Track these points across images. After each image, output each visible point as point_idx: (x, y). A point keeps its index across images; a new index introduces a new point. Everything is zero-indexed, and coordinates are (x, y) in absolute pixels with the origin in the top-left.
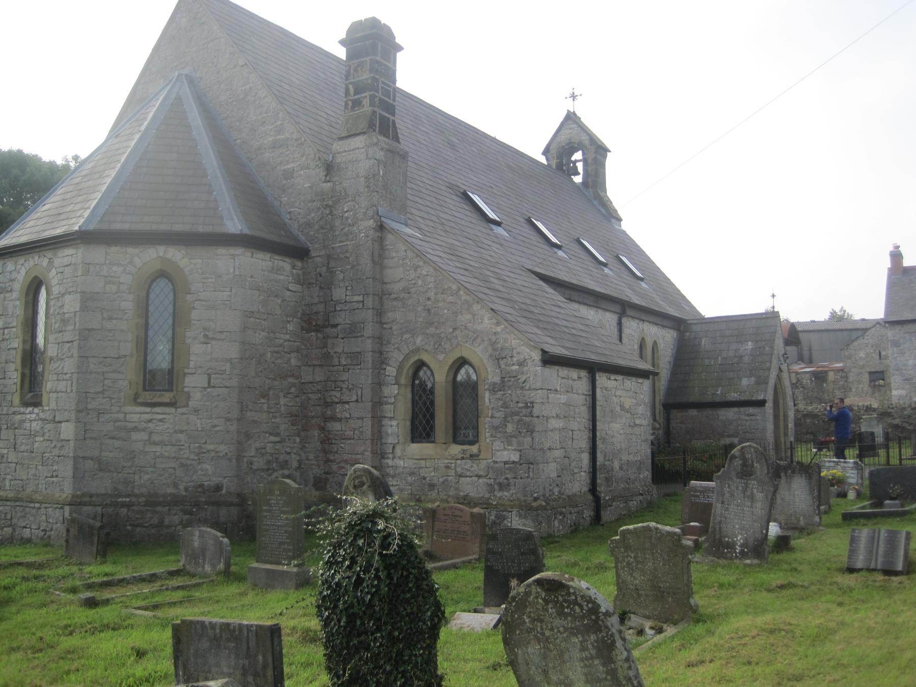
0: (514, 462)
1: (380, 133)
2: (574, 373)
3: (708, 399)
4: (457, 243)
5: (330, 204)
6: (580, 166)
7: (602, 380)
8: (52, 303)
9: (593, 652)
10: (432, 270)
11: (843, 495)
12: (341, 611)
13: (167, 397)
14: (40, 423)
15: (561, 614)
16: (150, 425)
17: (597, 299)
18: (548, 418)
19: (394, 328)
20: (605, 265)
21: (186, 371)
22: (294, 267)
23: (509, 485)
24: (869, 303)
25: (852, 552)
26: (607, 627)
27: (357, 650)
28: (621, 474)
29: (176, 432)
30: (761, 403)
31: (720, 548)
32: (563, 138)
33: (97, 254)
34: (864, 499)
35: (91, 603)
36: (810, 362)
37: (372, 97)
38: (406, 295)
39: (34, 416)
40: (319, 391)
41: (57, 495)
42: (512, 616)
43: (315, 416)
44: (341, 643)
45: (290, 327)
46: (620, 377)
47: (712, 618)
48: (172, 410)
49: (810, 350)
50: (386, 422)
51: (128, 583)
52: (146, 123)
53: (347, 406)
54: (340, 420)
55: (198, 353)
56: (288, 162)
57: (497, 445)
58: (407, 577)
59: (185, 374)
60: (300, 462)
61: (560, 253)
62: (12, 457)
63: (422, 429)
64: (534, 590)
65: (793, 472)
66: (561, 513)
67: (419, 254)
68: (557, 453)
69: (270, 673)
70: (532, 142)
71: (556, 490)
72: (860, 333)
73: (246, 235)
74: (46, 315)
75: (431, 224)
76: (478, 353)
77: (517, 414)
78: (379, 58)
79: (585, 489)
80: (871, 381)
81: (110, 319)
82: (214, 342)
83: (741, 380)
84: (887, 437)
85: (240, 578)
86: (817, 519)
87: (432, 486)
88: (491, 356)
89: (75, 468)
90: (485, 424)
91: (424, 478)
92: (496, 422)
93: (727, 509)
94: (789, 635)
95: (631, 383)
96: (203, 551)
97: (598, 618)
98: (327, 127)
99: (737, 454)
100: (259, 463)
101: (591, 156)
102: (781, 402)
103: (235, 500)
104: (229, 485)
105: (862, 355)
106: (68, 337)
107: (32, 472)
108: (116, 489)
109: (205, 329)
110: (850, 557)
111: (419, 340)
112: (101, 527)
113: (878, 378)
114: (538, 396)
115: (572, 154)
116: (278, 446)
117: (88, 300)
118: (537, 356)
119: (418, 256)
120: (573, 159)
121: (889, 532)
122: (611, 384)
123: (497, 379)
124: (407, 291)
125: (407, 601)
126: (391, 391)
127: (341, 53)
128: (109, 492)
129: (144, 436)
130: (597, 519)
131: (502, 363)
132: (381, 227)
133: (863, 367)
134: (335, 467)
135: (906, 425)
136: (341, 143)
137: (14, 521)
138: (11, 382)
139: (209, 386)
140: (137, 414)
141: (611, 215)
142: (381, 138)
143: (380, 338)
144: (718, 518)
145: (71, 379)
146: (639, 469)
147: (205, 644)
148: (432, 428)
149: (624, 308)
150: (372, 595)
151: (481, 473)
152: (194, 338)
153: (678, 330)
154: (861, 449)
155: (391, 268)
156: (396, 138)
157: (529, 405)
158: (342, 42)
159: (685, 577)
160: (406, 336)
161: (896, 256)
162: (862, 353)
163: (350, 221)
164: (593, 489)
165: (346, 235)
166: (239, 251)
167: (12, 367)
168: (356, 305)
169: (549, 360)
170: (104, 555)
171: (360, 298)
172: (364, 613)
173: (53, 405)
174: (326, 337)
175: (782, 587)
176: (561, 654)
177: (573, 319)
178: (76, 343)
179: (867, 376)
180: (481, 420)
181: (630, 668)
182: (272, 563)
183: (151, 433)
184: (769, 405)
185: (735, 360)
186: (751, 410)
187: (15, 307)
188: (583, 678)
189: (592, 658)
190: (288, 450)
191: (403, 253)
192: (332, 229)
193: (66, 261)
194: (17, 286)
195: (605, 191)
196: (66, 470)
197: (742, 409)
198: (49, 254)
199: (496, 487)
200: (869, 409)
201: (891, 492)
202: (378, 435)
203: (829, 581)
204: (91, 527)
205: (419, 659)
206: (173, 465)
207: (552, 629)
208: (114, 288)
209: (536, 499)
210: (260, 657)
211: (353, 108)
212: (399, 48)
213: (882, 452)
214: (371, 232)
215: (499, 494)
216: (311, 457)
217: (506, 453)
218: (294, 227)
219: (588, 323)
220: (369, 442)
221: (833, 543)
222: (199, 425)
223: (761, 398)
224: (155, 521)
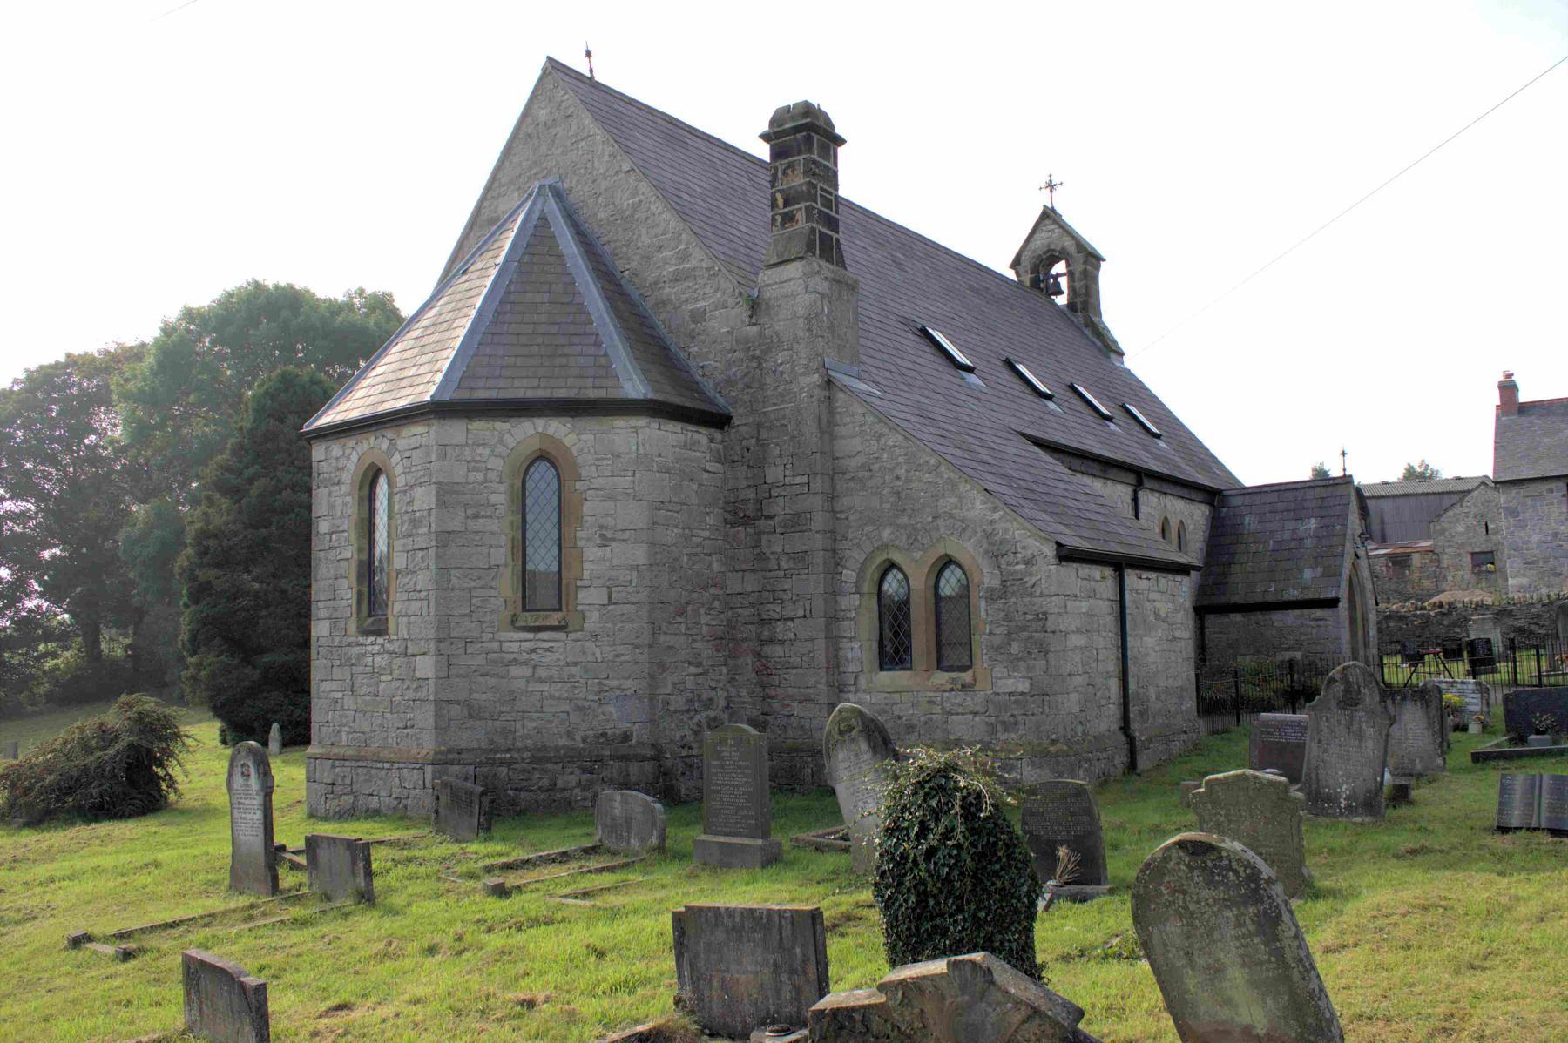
0: (1022, 693)
1: (821, 257)
2: (1096, 572)
3: (1258, 598)
4: (923, 400)
5: (758, 354)
6: (1063, 282)
7: (1132, 578)
8: (397, 498)
9: (1252, 928)
10: (901, 438)
11: (1463, 728)
12: (909, 890)
13: (554, 619)
14: (386, 656)
15: (1210, 883)
16: (533, 656)
17: (1106, 466)
18: (1067, 633)
19: (852, 518)
20: (1049, 397)
21: (579, 583)
22: (711, 440)
23: (1016, 723)
24: (1467, 453)
25: (1503, 806)
26: (1270, 897)
27: (930, 936)
28: (1159, 705)
29: (568, 664)
30: (1333, 603)
31: (1320, 802)
32: (1039, 243)
33: (456, 430)
34: (1493, 733)
35: (501, 892)
36: (1383, 540)
37: (809, 210)
38: (867, 474)
39: (377, 648)
40: (752, 605)
41: (414, 751)
42: (1146, 887)
43: (747, 638)
44: (909, 929)
45: (710, 520)
46: (1153, 575)
47: (1332, 893)
48: (561, 635)
49: (1382, 522)
50: (845, 644)
51: (535, 865)
52: (504, 253)
53: (790, 624)
54: (782, 642)
55: (593, 559)
56: (696, 300)
57: (999, 671)
58: (995, 843)
59: (577, 587)
60: (729, 699)
61: (1051, 405)
62: (349, 702)
63: (894, 653)
64: (1174, 855)
65: (1404, 699)
66: (1088, 760)
67: (883, 418)
68: (1079, 680)
69: (812, 969)
70: (996, 249)
71: (1080, 729)
72: (1455, 498)
73: (652, 401)
74: (390, 517)
75: (887, 374)
76: (967, 549)
77: (1024, 629)
78: (815, 157)
79: (1115, 727)
80: (1474, 566)
81: (476, 517)
82: (614, 544)
83: (1301, 571)
84: (1512, 647)
85: (680, 856)
86: (1440, 761)
88: (987, 552)
89: (438, 715)
90: (980, 641)
91: (900, 718)
92: (997, 641)
93: (1326, 751)
94: (1449, 913)
95: (1166, 581)
96: (628, 821)
97: (1258, 886)
98: (743, 250)
99: (1338, 677)
100: (678, 702)
101: (1079, 268)
102: (1358, 599)
103: (649, 752)
104: (640, 733)
105: (1460, 529)
106: (421, 542)
107: (378, 721)
108: (492, 742)
109: (601, 527)
110: (1501, 812)
112: (483, 794)
113: (1484, 561)
114: (1053, 605)
115: (1051, 265)
116: (700, 679)
117: (447, 495)
118: (1049, 551)
119: (881, 421)
120: (1053, 272)
121: (1555, 778)
122: (1143, 584)
123: (996, 583)
124: (866, 467)
125: (996, 874)
126: (849, 602)
127: (763, 151)
128: (483, 745)
129: (527, 671)
130: (1132, 766)
131: (1002, 561)
132: (829, 383)
133: (1462, 546)
134: (776, 706)
135: (1533, 627)
136: (769, 272)
137: (355, 787)
138: (345, 603)
139: (610, 602)
140: (516, 642)
141: (1108, 348)
142: (823, 263)
143: (833, 532)
144: (1314, 762)
145: (427, 598)
146: (1181, 698)
147: (720, 935)
148: (908, 650)
149: (1140, 477)
150: (951, 868)
151: (977, 709)
152: (589, 539)
153: (1211, 504)
154: (1473, 663)
155: (843, 437)
156: (841, 263)
157: (1042, 617)
158: (765, 137)
159: (1296, 840)
160: (868, 528)
161: (1508, 388)
162: (1460, 527)
163: (786, 376)
164: (1125, 727)
165: (782, 395)
166: (642, 421)
167: (345, 583)
168: (797, 490)
169: (1067, 555)
170: (489, 829)
171: (805, 479)
172: (941, 891)
173: (404, 633)
174: (759, 534)
175: (1414, 852)
176: (1210, 933)
177: (1083, 498)
178: (432, 552)
179: (1468, 559)
180: (975, 638)
181: (1300, 947)
182: (726, 834)
183: (534, 667)
184: (1343, 605)
185: (1293, 544)
186: (1319, 612)
187: (345, 504)
188: (1239, 960)
189: (1251, 935)
190: (713, 684)
191: (859, 418)
192: (762, 386)
193: (414, 442)
194: (346, 477)
195: (1100, 315)
196: (425, 717)
197: (1306, 611)
198: (390, 434)
199: (999, 727)
200: (1479, 607)
201: (1530, 721)
202: (835, 663)
203: (1475, 843)
204: (470, 793)
205: (1014, 945)
206: (567, 708)
207: (1198, 902)
208: (480, 476)
209: (1054, 742)
210: (798, 950)
211: (783, 225)
212: (840, 141)
213: (1501, 666)
214: (817, 391)
215: (1002, 736)
216: (744, 692)
217: (1010, 681)
218: (709, 387)
219: (1101, 501)
220: (822, 672)
221: (1476, 794)
222: (598, 655)
223: (1332, 595)
224: (545, 782)
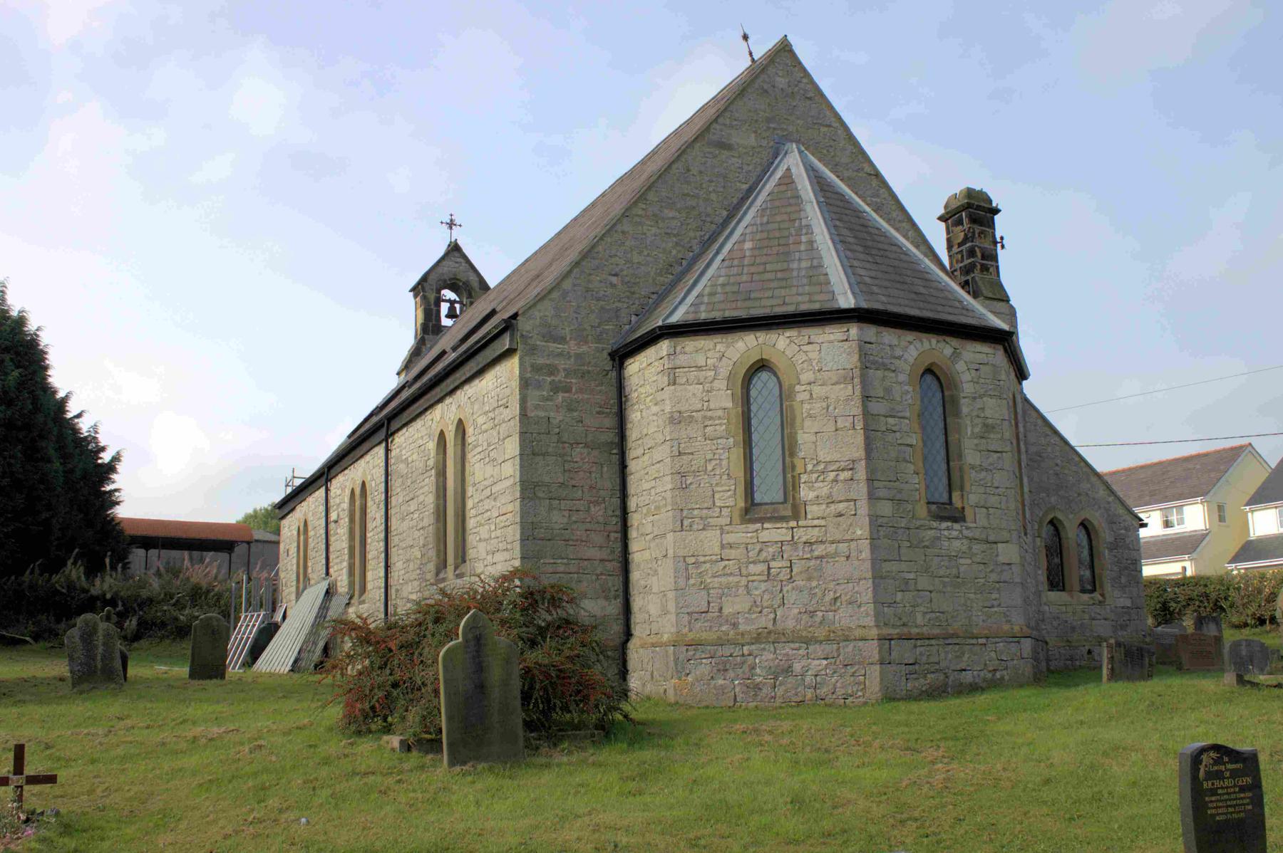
57: (1117, 593)
87: (1073, 629)
111: (1053, 499)
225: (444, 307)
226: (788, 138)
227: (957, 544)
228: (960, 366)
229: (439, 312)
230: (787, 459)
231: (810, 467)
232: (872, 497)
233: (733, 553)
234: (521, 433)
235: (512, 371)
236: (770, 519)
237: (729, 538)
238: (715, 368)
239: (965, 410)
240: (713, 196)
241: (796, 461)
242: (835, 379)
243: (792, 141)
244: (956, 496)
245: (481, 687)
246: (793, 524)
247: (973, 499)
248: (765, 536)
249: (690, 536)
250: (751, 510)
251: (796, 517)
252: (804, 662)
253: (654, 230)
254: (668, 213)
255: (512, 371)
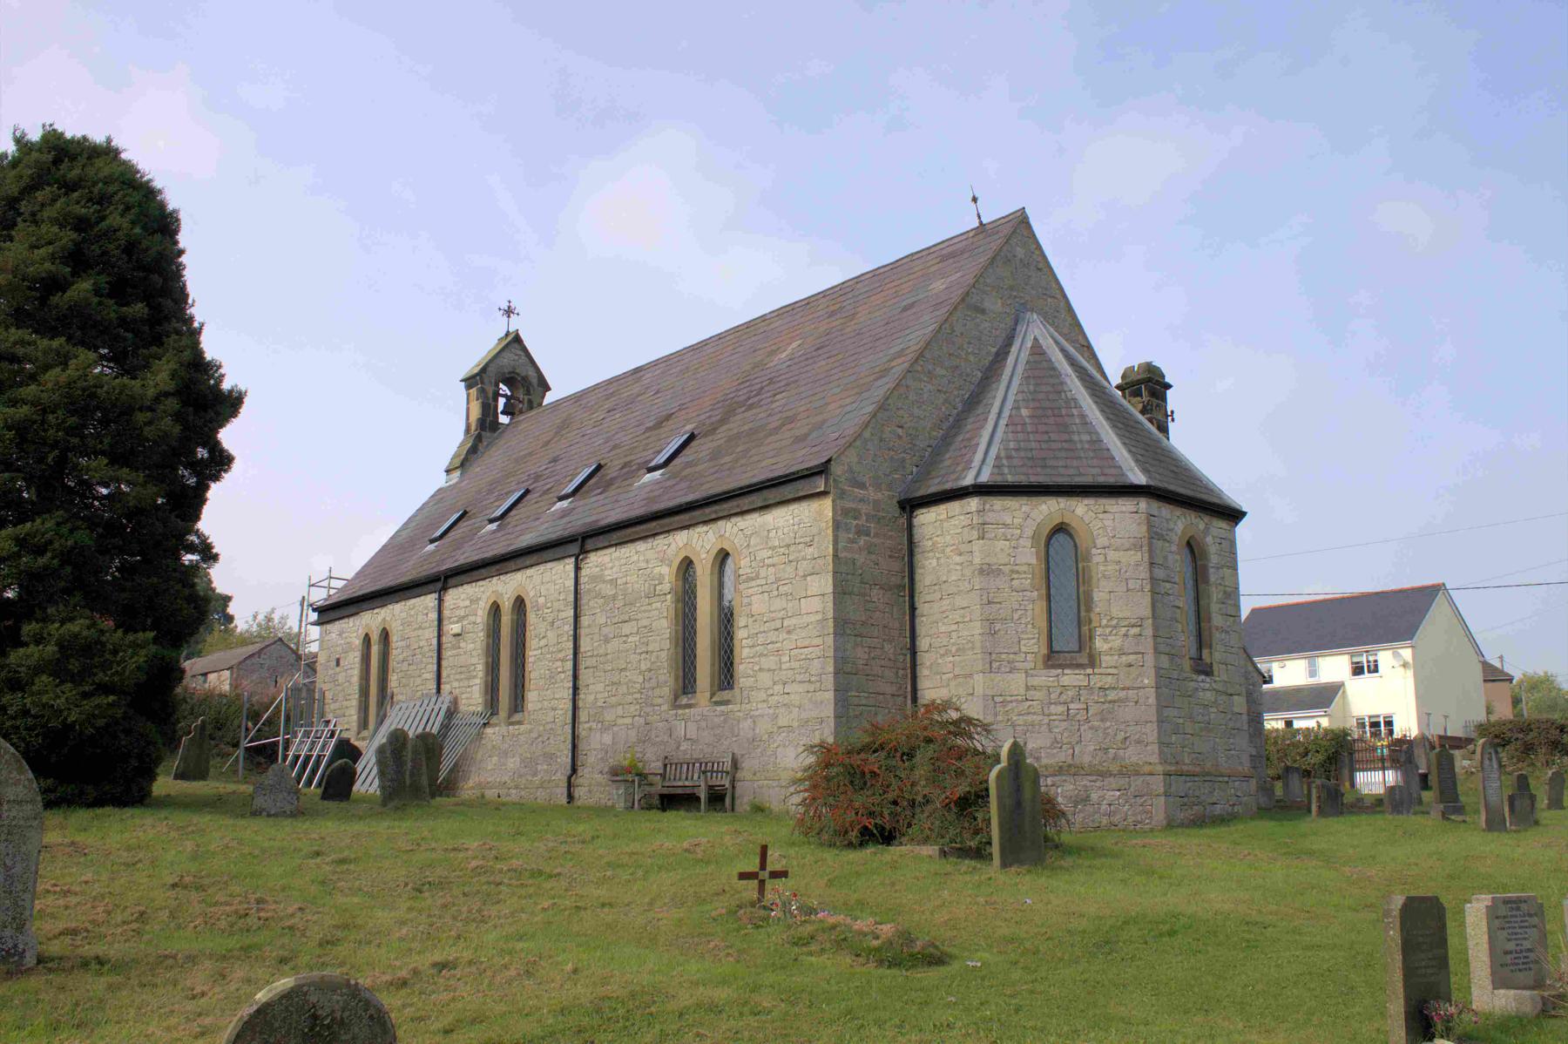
225: (502, 401)
226: (1025, 307)
227: (1208, 694)
228: (1209, 540)
229: (496, 407)
230: (1083, 614)
231: (1104, 622)
232: (1156, 651)
233: (1037, 695)
234: (835, 573)
235: (820, 513)
236: (1071, 666)
237: (1035, 681)
238: (1021, 527)
239: (1212, 579)
240: (971, 358)
241: (1092, 615)
242: (1127, 546)
243: (1032, 310)
244: (1205, 652)
245: (1019, 804)
246: (1089, 671)
247: (1217, 656)
248: (1066, 680)
249: (998, 677)
250: (1053, 658)
251: (1092, 664)
252: (1101, 793)
253: (930, 386)
254: (940, 371)
255: (820, 513)
